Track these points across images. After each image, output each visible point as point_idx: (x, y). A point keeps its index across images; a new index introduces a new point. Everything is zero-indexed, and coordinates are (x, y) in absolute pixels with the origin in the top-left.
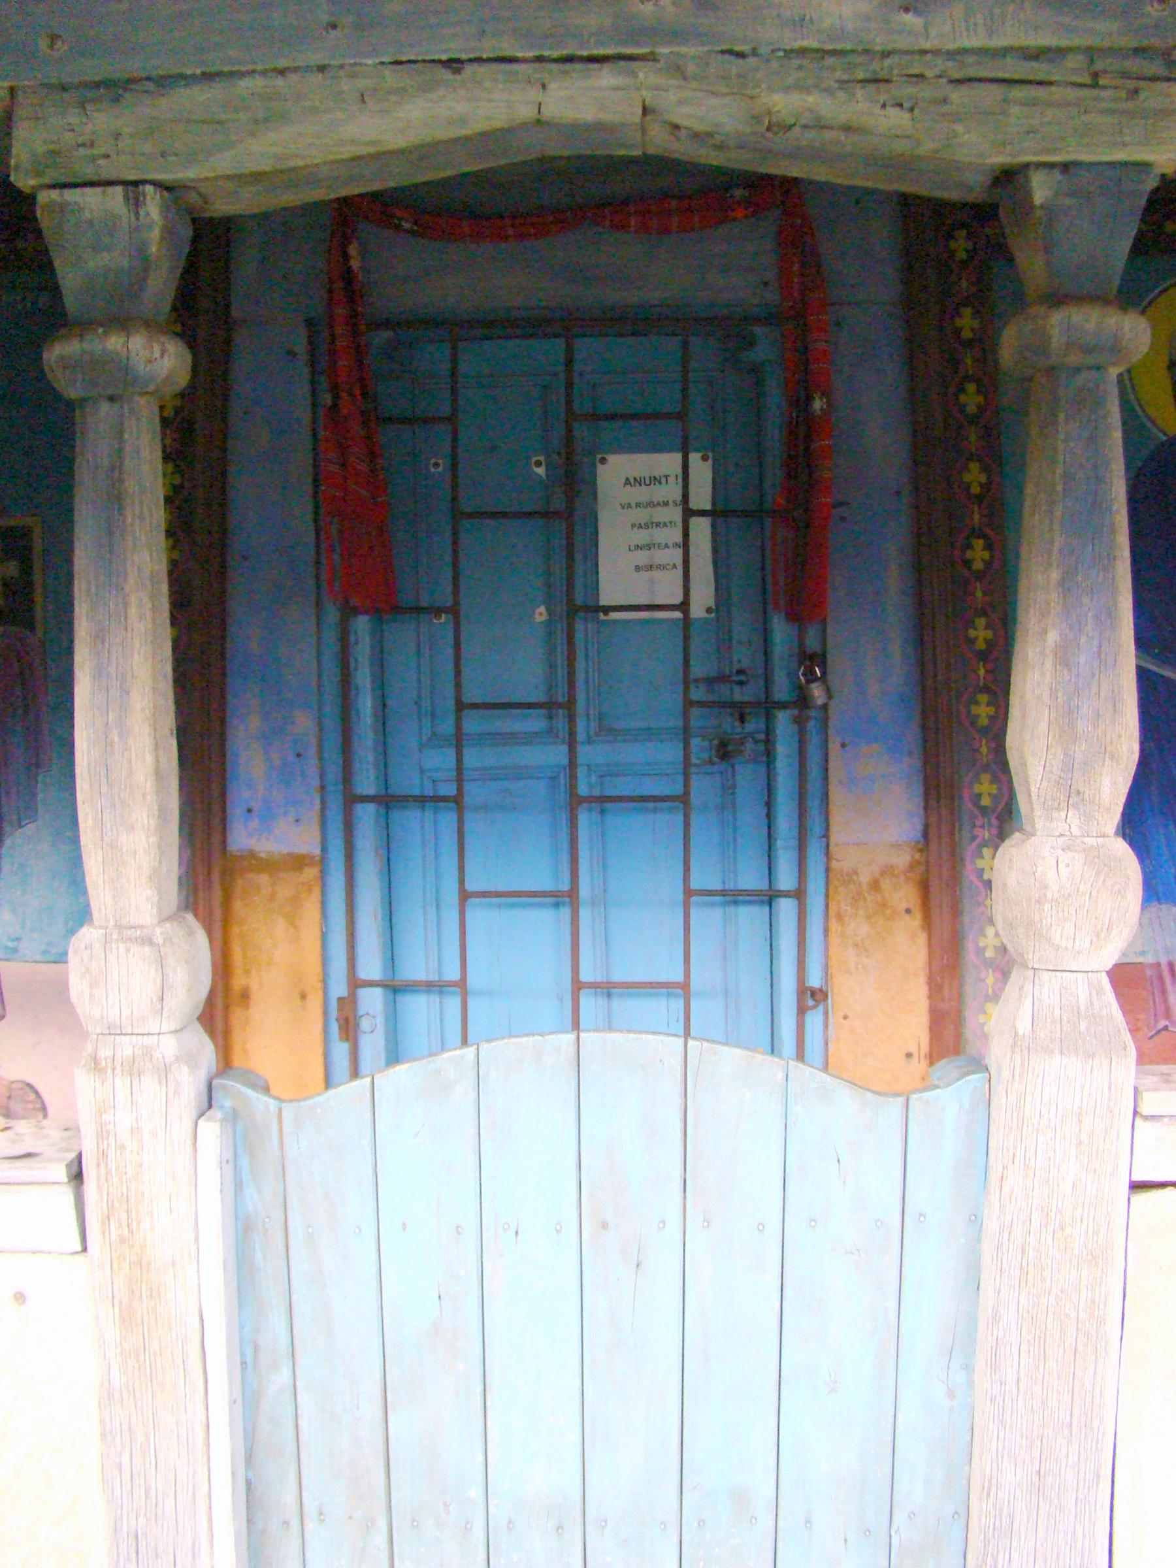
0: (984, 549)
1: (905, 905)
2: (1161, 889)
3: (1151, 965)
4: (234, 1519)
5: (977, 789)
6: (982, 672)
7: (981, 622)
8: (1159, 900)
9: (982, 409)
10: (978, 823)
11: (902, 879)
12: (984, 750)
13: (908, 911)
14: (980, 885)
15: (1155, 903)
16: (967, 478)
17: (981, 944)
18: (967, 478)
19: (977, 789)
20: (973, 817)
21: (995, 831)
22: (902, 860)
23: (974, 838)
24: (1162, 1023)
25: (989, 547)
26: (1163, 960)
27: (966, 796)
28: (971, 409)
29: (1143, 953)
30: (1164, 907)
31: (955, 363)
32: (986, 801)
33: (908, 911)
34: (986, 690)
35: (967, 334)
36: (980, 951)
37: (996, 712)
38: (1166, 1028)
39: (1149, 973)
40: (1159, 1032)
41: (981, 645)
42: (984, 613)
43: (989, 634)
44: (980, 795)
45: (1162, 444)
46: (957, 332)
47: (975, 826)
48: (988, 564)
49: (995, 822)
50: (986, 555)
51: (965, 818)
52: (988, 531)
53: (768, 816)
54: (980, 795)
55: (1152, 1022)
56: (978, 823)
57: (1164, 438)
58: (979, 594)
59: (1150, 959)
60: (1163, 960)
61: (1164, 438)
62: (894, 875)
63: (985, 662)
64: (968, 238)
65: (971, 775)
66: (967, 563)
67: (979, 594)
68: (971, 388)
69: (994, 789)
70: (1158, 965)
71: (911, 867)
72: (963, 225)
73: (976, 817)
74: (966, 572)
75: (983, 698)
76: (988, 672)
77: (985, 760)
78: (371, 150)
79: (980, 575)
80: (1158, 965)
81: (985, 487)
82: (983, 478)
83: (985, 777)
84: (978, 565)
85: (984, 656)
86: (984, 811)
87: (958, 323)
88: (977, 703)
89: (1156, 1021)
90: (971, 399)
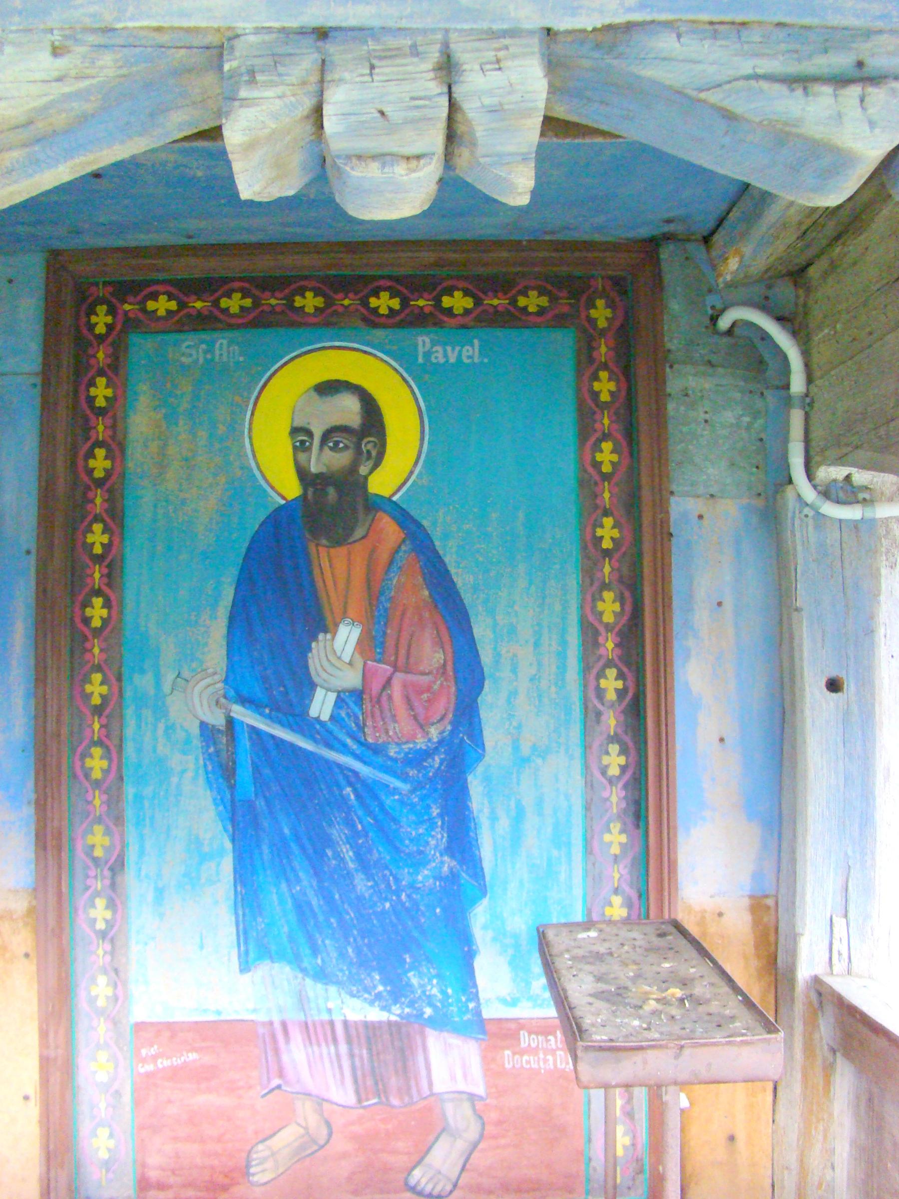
0: (103, 607)
1: (24, 949)
2: (273, 948)
3: (264, 1024)
4: (831, 988)
5: (90, 840)
6: (96, 726)
7: (97, 677)
8: (271, 958)
9: (108, 473)
10: (92, 873)
11: (21, 924)
12: (97, 802)
13: (27, 955)
14: (92, 934)
15: (268, 961)
16: (90, 539)
17: (93, 993)
18: (90, 539)
19: (90, 840)
20: (86, 867)
21: (108, 882)
22: (20, 905)
23: (87, 888)
24: (276, 1082)
25: (107, 604)
26: (276, 1019)
27: (79, 847)
28: (99, 474)
29: (255, 1010)
30: (276, 965)
31: (88, 428)
32: (98, 853)
33: (27, 955)
34: (100, 743)
35: (100, 402)
36: (93, 1000)
37: (109, 766)
38: (279, 1087)
39: (261, 1030)
40: (273, 1090)
41: (96, 700)
42: (99, 669)
43: (104, 689)
44: (93, 846)
45: (280, 508)
46: (91, 400)
47: (88, 877)
48: (105, 621)
49: (107, 873)
50: (105, 613)
51: (79, 866)
52: (106, 590)
53: (635, 708)
54: (93, 846)
55: (265, 1078)
56: (92, 873)
57: (283, 502)
58: (96, 650)
59: (262, 1017)
60: (276, 1019)
61: (283, 502)
62: (11, 918)
63: (100, 716)
64: (317, 309)
65: (85, 825)
66: (87, 621)
67: (96, 650)
68: (100, 453)
69: (107, 841)
70: (271, 1023)
71: (31, 911)
72: (103, 301)
73: (89, 868)
74: (85, 629)
75: (97, 751)
76: (102, 726)
77: (98, 814)
78: (184, 241)
79: (98, 632)
80: (271, 1023)
81: (107, 547)
82: (105, 539)
83: (99, 829)
84: (96, 623)
85: (98, 710)
86: (96, 860)
87: (93, 391)
88: (91, 756)
89: (269, 1080)
90: (100, 463)
